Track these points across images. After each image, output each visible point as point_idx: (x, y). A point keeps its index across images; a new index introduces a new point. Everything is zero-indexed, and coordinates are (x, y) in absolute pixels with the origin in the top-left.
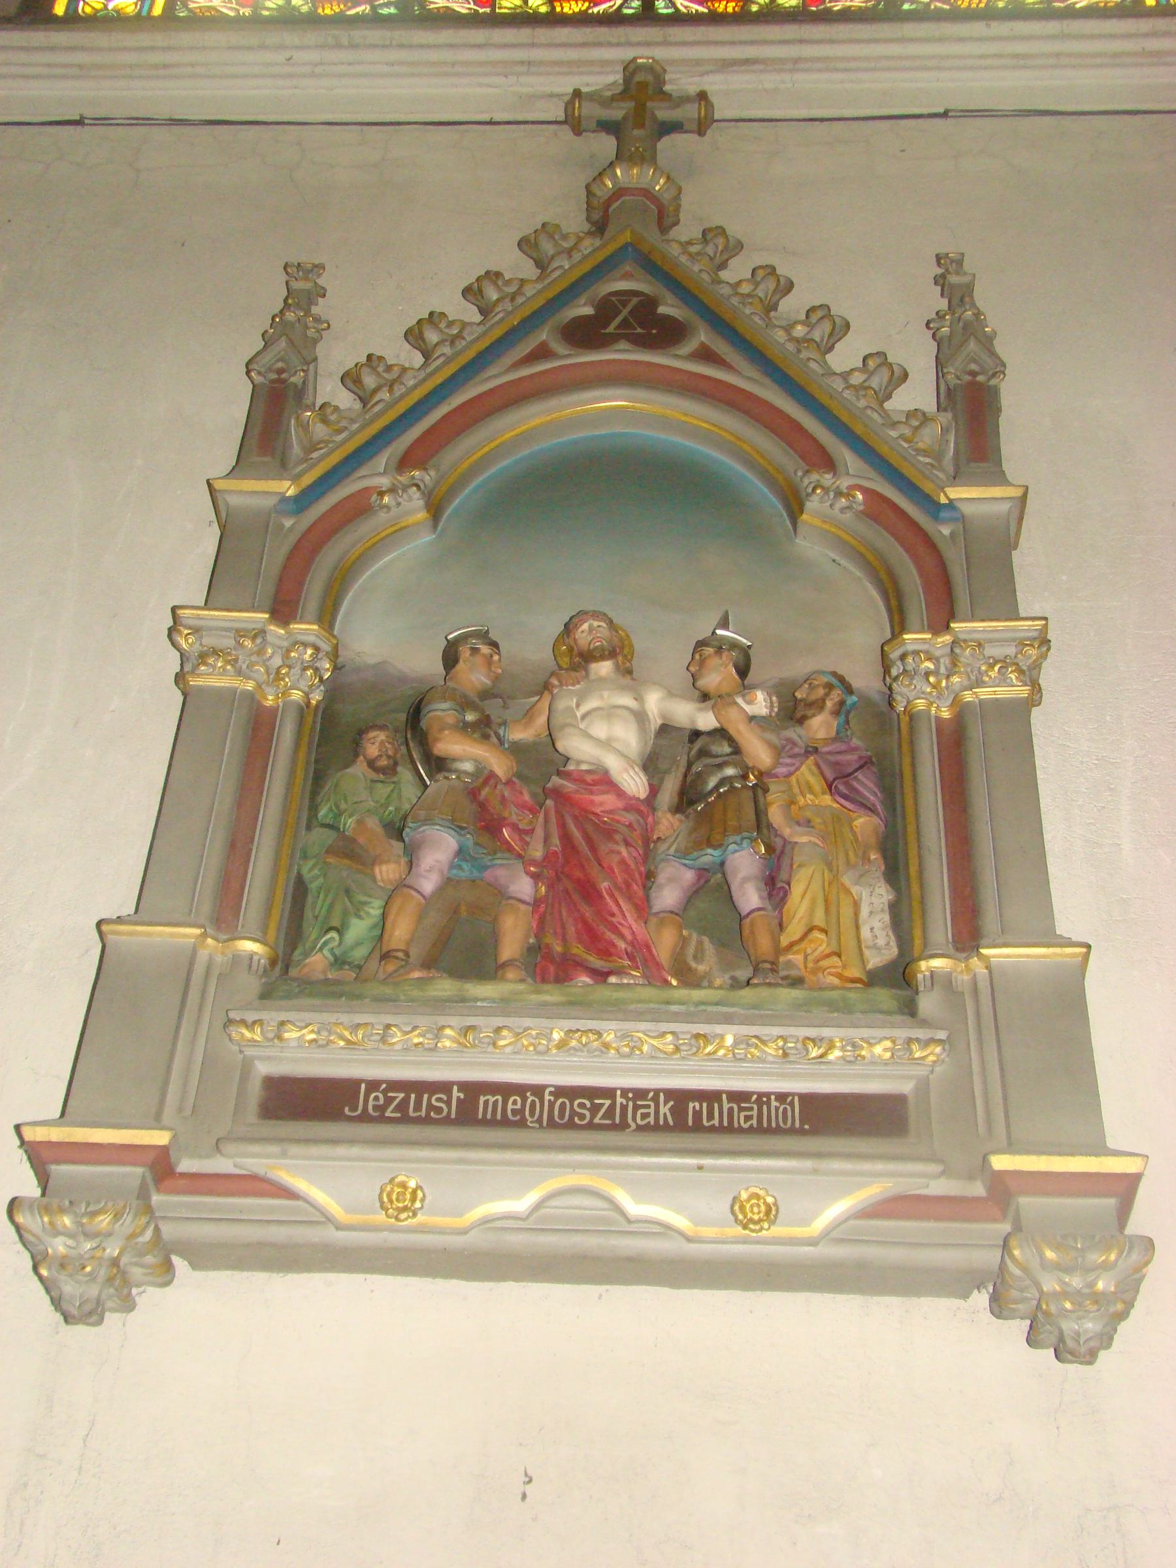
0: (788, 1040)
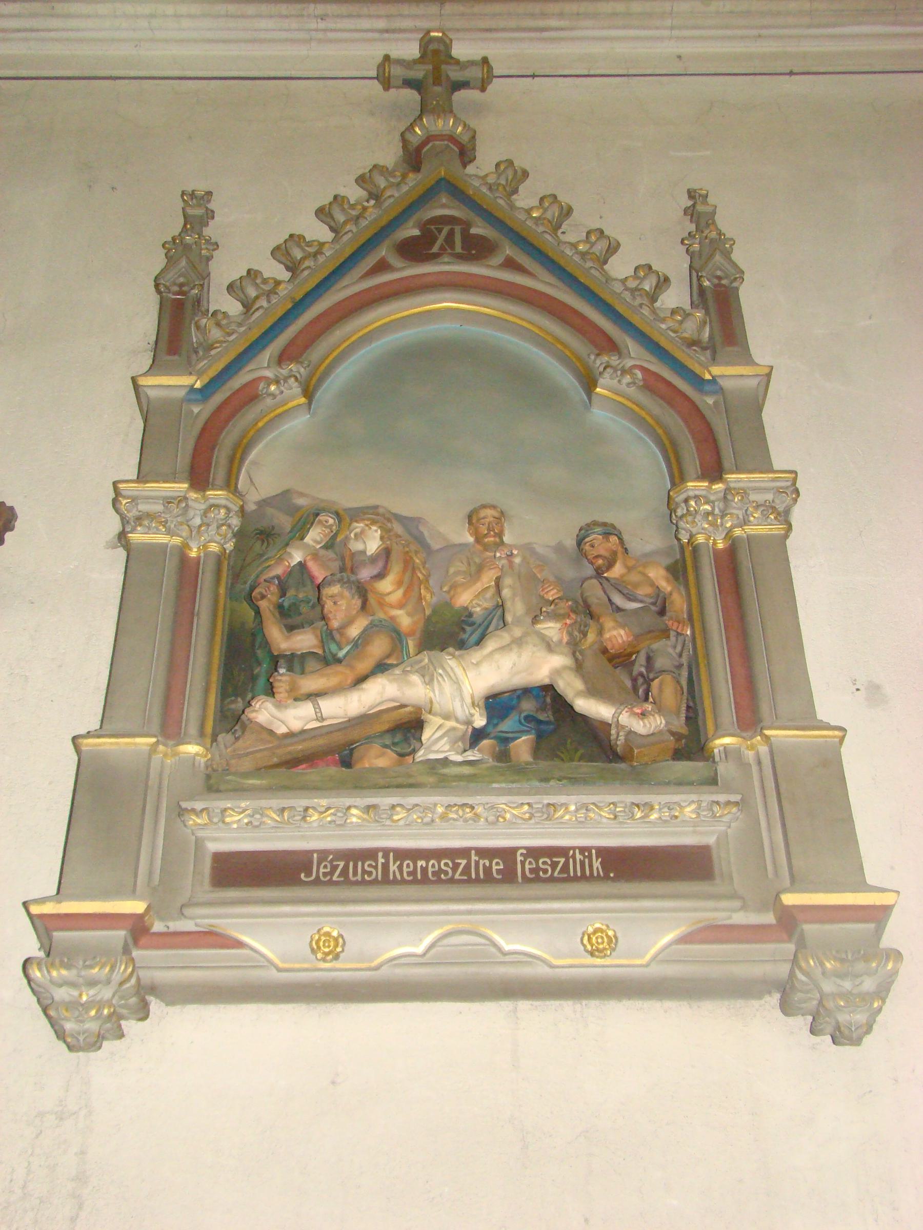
0: (618, 805)
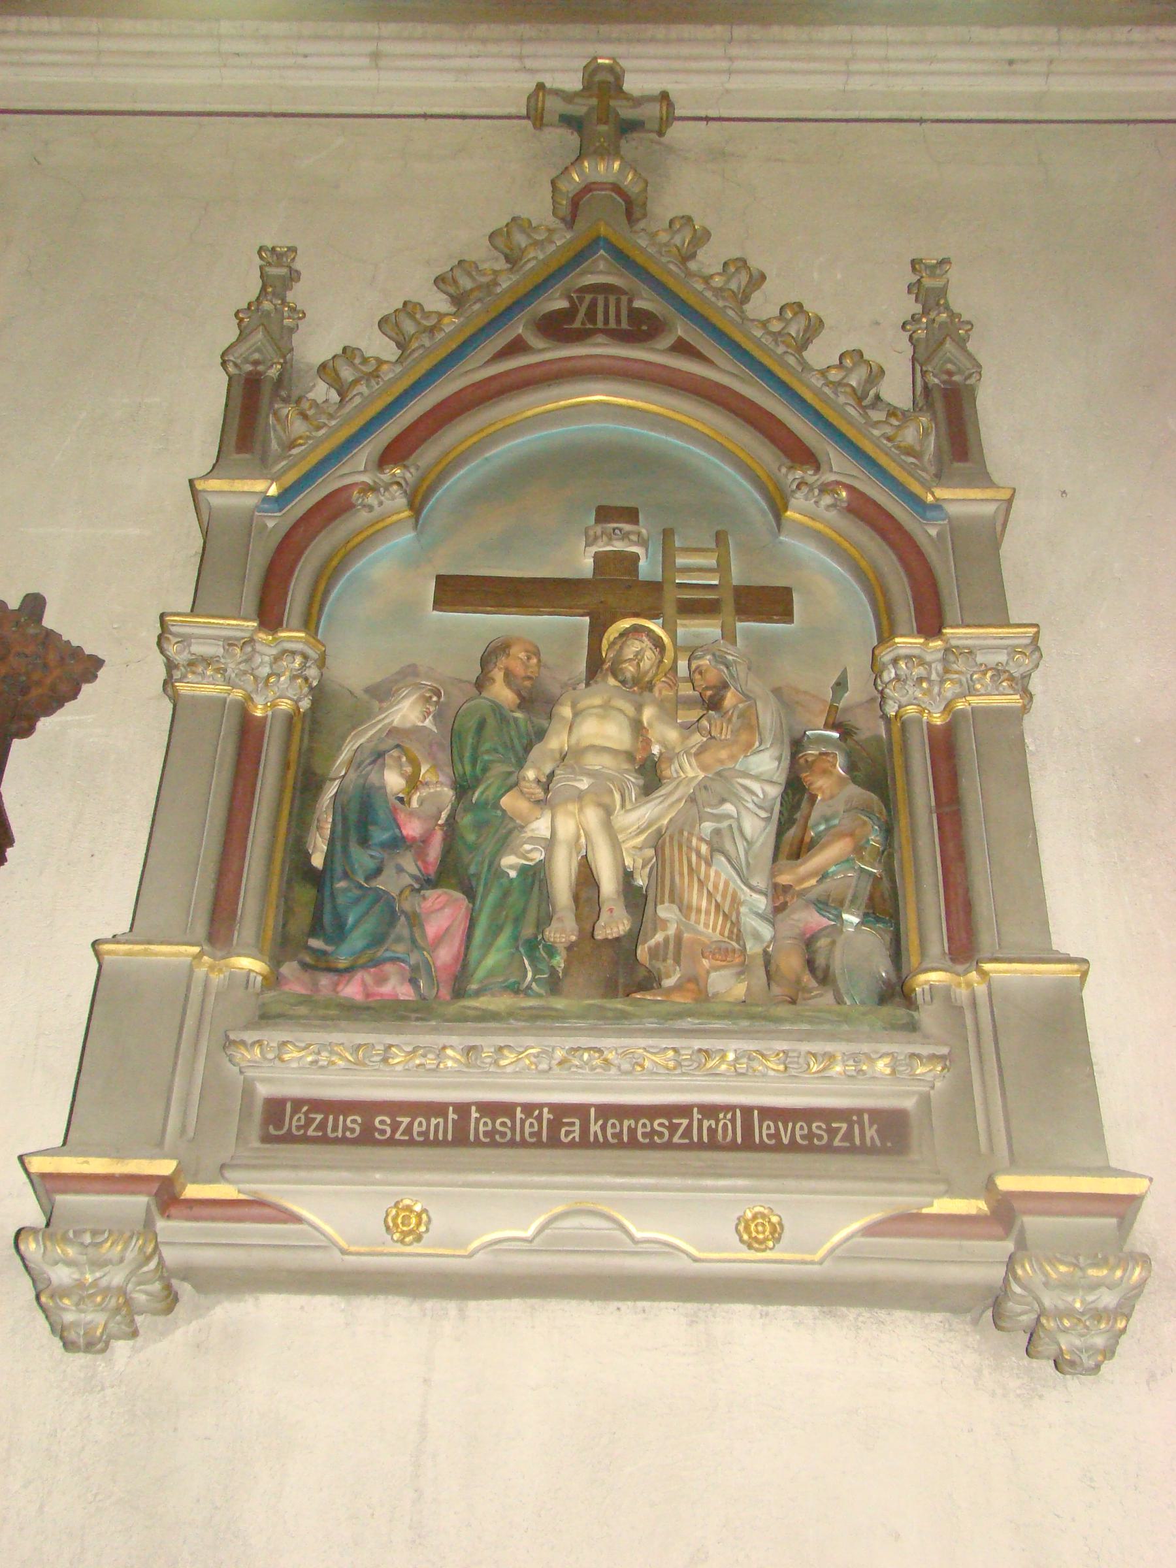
0: (790, 1054)
